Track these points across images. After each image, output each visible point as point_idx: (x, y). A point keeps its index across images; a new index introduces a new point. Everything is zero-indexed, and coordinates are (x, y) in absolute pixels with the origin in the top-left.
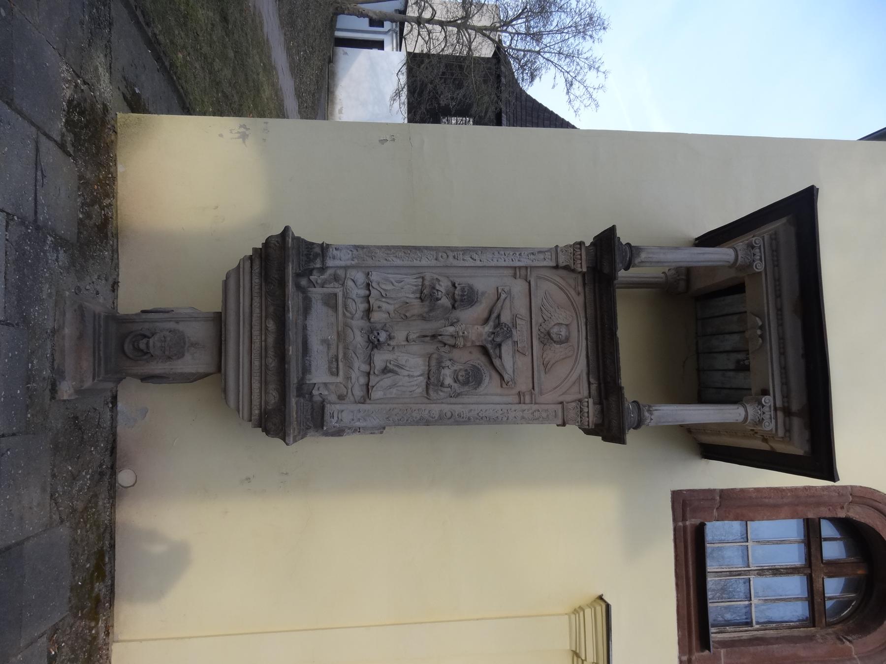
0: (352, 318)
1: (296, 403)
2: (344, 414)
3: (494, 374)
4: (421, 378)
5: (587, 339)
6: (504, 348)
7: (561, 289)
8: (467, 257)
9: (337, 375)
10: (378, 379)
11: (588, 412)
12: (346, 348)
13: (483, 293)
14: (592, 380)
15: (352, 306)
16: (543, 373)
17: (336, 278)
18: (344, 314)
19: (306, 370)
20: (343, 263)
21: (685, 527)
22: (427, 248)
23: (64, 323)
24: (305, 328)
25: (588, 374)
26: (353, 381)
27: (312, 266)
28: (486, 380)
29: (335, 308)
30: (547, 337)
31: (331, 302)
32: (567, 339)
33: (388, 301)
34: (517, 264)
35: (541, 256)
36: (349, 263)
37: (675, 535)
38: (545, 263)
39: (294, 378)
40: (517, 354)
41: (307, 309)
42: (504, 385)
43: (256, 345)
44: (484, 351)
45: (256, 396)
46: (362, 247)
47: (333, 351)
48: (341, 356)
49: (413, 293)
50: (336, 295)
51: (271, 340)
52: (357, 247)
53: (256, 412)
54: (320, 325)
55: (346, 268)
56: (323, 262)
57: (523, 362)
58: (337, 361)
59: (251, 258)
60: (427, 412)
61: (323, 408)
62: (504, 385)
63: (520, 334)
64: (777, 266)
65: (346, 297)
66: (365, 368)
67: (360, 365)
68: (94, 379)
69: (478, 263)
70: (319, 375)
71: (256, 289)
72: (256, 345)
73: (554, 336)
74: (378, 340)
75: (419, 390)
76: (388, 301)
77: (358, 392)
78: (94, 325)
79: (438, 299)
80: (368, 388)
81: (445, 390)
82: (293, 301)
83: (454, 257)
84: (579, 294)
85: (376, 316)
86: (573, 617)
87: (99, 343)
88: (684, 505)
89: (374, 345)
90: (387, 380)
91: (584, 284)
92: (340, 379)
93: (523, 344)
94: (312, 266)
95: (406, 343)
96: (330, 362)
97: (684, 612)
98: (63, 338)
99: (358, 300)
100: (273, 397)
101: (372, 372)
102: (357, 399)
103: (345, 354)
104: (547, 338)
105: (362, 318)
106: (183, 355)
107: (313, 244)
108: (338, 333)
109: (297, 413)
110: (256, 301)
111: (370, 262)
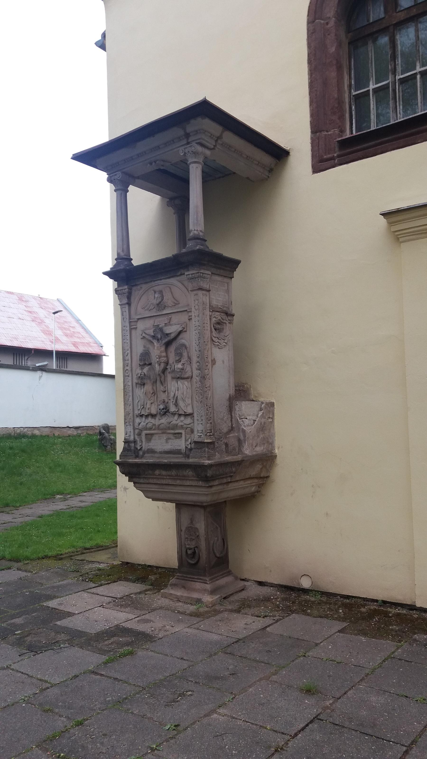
0: (155, 425)
1: (192, 458)
2: (199, 429)
3: (181, 336)
4: (179, 382)
5: (161, 280)
6: (168, 332)
7: (140, 299)
8: (127, 358)
9: (181, 433)
10: (180, 409)
11: (192, 274)
12: (169, 428)
13: (145, 347)
14: (179, 273)
15: (149, 425)
16: (180, 305)
17: (139, 435)
18: (154, 430)
19: (178, 452)
20: (132, 431)
21: (339, 156)
22: (124, 382)
23: (175, 595)
24: (161, 453)
25: (178, 276)
26: (183, 424)
27: (133, 448)
28: (183, 341)
29: (152, 435)
30: (160, 305)
31: (149, 437)
32: (161, 292)
33: (145, 404)
34: (128, 328)
35: (124, 313)
36: (132, 427)
37: (345, 164)
38: (127, 311)
39: (180, 460)
40: (171, 323)
41: (152, 451)
42: (185, 329)
43: (170, 482)
44: (168, 344)
45: (188, 483)
46: (125, 419)
47: (171, 436)
48: (172, 431)
49: (141, 389)
50: (146, 434)
51: (164, 473)
52: (125, 423)
53: (200, 483)
54: (160, 444)
55: (134, 429)
56: (131, 442)
57: (175, 319)
58: (175, 434)
59: (134, 483)
60: (197, 378)
61: (196, 442)
62: (185, 329)
63: (161, 322)
64: (173, 141)
65: (146, 429)
66: (176, 417)
67: (175, 420)
68: (207, 584)
69: (129, 351)
70: (181, 444)
71: (146, 481)
72: (170, 482)
73: (159, 300)
74: (163, 409)
75: (186, 383)
76: (145, 404)
77: (188, 420)
78: (181, 579)
79: (145, 375)
80: (186, 415)
81: (185, 367)
82: (149, 459)
83: (127, 366)
84: (141, 288)
85: (154, 411)
86: (401, 240)
87: (190, 578)
88: (322, 161)
89: (165, 412)
90: (181, 404)
91: (136, 285)
92: (183, 432)
93: (165, 320)
94: (133, 448)
95: (166, 392)
96: (176, 438)
97: (359, 154)
98: (182, 596)
99: (147, 421)
100: (189, 473)
101: (178, 413)
102: (192, 421)
103: (173, 429)
104: (160, 306)
105: (155, 419)
106: (197, 529)
107: (124, 448)
108: (163, 433)
109: (196, 458)
110: (151, 481)
111: (131, 415)
